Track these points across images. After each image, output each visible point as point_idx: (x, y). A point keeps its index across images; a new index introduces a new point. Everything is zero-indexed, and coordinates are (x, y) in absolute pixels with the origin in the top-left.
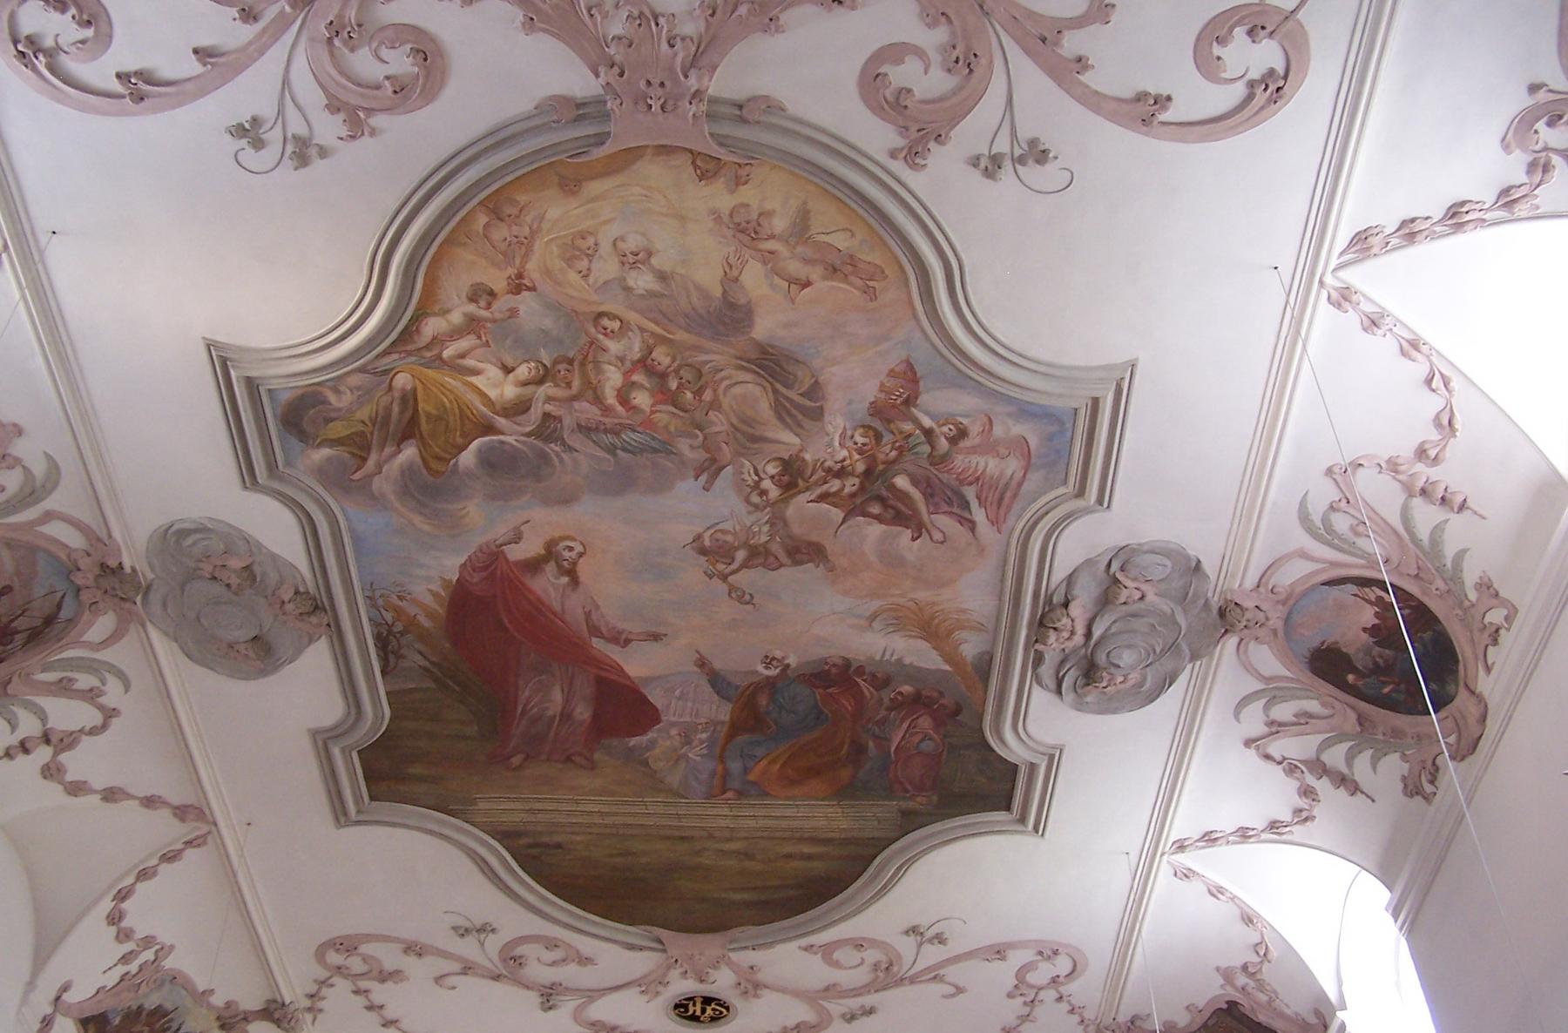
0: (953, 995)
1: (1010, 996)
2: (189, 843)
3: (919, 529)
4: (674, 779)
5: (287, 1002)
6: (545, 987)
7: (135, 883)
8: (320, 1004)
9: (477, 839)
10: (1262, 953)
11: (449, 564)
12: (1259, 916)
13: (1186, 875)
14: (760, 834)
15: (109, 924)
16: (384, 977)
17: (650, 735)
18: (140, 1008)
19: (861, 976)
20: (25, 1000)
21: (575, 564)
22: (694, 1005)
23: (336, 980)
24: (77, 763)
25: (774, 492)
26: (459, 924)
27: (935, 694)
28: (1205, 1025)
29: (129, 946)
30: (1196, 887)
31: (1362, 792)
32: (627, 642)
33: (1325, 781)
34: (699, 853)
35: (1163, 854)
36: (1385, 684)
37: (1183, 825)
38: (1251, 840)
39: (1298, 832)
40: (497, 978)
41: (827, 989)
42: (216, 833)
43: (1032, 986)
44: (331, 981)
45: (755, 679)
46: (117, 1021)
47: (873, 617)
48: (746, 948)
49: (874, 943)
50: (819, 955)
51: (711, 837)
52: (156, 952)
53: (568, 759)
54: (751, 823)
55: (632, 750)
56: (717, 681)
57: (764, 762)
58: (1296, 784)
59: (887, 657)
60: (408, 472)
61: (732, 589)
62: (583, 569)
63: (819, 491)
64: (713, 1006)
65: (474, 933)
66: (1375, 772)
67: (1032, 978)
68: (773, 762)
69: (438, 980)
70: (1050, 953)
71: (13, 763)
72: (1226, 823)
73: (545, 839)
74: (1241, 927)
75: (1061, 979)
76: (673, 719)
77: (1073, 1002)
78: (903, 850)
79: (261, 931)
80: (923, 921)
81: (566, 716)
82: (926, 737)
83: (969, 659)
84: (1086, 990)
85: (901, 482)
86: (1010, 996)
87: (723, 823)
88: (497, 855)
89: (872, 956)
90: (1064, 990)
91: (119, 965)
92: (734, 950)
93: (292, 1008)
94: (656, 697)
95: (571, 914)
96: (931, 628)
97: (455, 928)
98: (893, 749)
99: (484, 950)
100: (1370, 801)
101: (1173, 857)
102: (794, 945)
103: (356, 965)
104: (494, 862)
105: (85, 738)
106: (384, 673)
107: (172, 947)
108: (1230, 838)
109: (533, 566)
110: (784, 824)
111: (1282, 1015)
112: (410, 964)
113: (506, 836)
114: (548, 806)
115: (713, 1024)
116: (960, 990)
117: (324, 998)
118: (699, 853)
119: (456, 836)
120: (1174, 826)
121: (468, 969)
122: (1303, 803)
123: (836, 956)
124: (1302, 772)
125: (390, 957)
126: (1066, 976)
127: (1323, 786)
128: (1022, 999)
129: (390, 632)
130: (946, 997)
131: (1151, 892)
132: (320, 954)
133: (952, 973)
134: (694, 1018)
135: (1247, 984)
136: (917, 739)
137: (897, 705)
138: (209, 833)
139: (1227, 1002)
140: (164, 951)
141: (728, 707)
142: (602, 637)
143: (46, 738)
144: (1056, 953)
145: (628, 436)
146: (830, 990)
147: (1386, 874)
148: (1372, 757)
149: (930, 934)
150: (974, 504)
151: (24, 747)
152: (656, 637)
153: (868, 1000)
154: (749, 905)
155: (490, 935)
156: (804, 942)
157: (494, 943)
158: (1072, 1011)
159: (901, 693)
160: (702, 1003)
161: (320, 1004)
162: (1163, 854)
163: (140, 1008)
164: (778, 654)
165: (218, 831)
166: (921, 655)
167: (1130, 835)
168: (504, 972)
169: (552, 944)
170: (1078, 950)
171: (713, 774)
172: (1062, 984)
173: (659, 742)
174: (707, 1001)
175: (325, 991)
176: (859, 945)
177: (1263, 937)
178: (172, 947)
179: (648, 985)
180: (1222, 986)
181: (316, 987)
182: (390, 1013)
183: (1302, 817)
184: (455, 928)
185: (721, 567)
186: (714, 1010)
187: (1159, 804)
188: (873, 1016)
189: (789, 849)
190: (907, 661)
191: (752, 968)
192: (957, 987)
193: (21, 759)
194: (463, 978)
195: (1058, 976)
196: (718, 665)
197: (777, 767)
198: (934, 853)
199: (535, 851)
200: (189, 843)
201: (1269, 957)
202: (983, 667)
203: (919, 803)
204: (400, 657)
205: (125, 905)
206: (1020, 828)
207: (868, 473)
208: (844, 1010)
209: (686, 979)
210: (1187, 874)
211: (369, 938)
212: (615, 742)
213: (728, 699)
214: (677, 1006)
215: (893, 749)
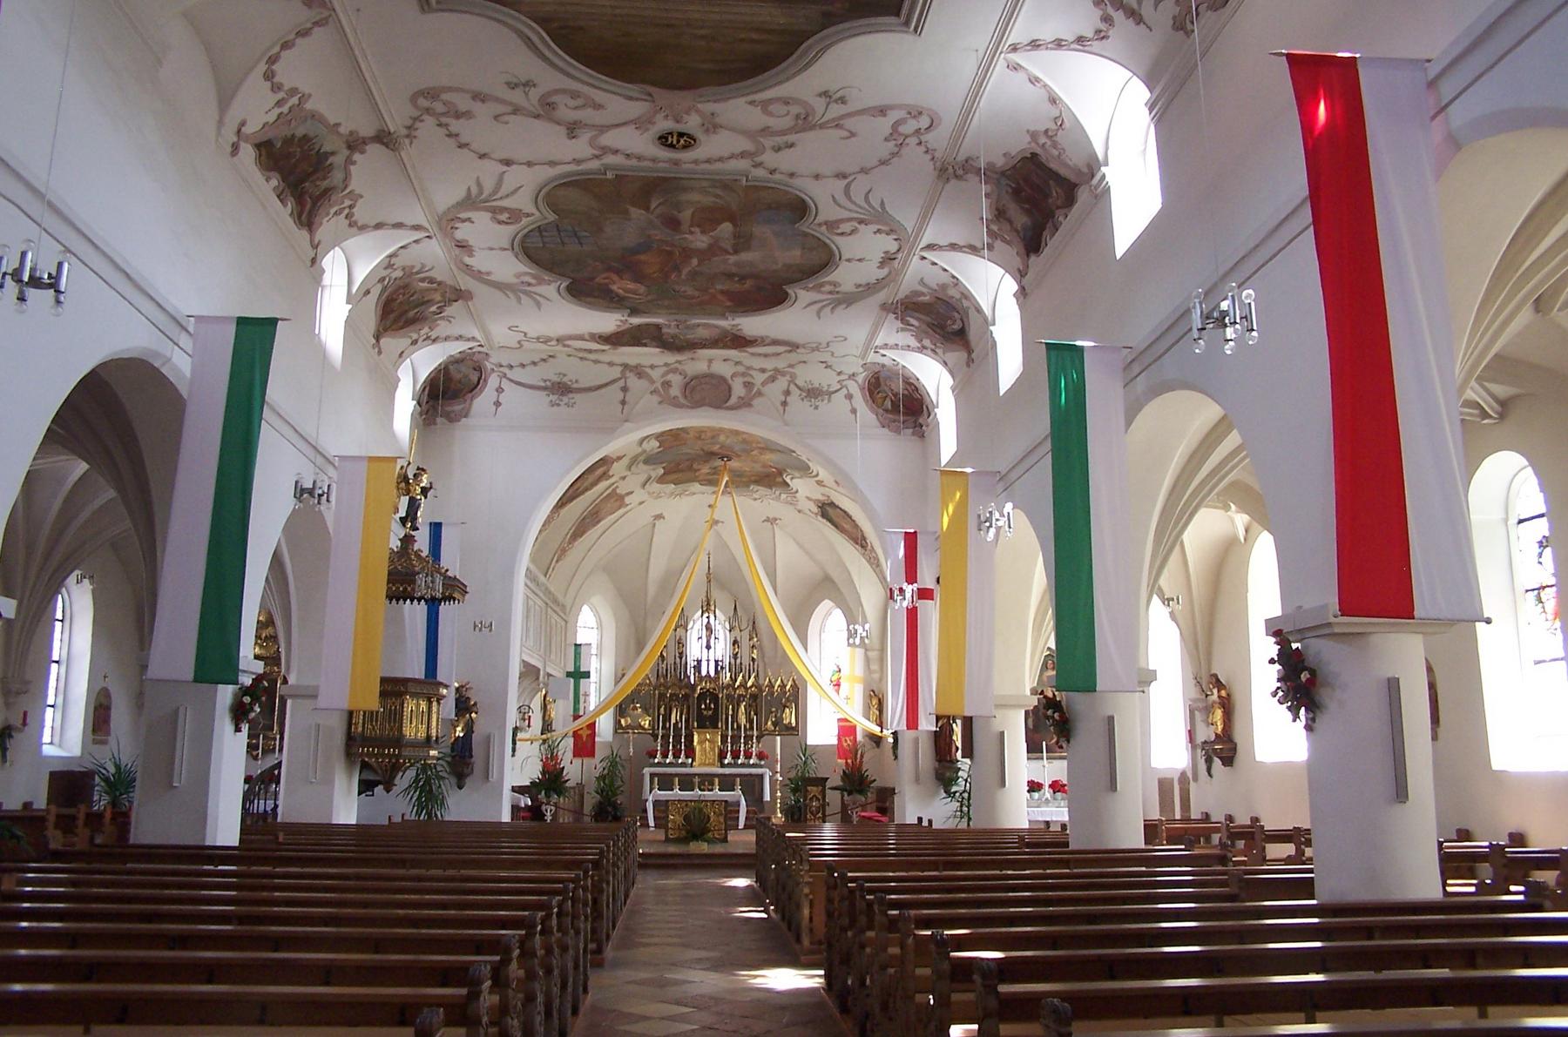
0: (847, 138)
1: (886, 139)
2: (316, 24)
5: (392, 131)
6: (570, 124)
7: (281, 51)
8: (414, 133)
9: (524, 23)
10: (1059, 124)
12: (1060, 99)
13: (1015, 68)
15: (265, 80)
16: (458, 115)
19: (787, 122)
20: (219, 133)
22: (672, 137)
23: (425, 117)
26: (510, 80)
28: (1014, 167)
29: (281, 95)
30: (1021, 76)
31: (1144, 23)
33: (1121, 12)
35: (1001, 53)
37: (1017, 34)
38: (1064, 48)
39: (1096, 46)
40: (537, 117)
41: (763, 130)
42: (334, 16)
43: (900, 134)
44: (421, 118)
46: (279, 145)
48: (709, 101)
49: (797, 101)
50: (759, 108)
52: (300, 98)
58: (1101, 13)
64: (685, 138)
65: (522, 87)
66: (1156, 10)
67: (901, 129)
69: (496, 117)
70: (916, 113)
72: (1047, 35)
74: (1047, 105)
75: (922, 131)
77: (929, 146)
78: (822, 39)
80: (833, 87)
84: (939, 139)
86: (886, 139)
88: (538, 34)
89: (795, 109)
90: (923, 138)
91: (276, 108)
92: (700, 102)
93: (395, 136)
95: (587, 74)
97: (508, 84)
100: (1148, 30)
101: (1009, 55)
102: (741, 101)
103: (439, 107)
104: (535, 39)
107: (310, 95)
108: (1049, 46)
111: (1066, 165)
112: (477, 108)
113: (543, 21)
115: (685, 150)
116: (853, 135)
117: (417, 129)
119: (510, 21)
121: (516, 111)
122: (1103, 26)
123: (771, 108)
124: (1106, 5)
125: (463, 103)
126: (926, 129)
127: (1118, 16)
128: (894, 142)
130: (844, 138)
131: (996, 64)
132: (414, 99)
133: (848, 123)
134: (672, 146)
135: (1046, 143)
138: (330, 16)
139: (1031, 153)
140: (304, 98)
144: (920, 113)
146: (766, 131)
147: (1149, 82)
149: (834, 97)
153: (791, 138)
155: (533, 88)
156: (750, 98)
157: (535, 94)
158: (927, 152)
160: (678, 136)
161: (414, 133)
163: (293, 135)
165: (336, 15)
167: (981, 39)
168: (542, 113)
169: (575, 95)
170: (936, 113)
172: (922, 134)
174: (681, 135)
175: (418, 124)
176: (786, 102)
177: (1061, 113)
178: (310, 95)
179: (640, 123)
180: (1029, 143)
181: (411, 122)
182: (463, 140)
183: (1101, 35)
184: (508, 84)
186: (685, 141)
187: (1000, 26)
188: (792, 149)
191: (713, 114)
192: (851, 132)
194: (513, 117)
195: (920, 129)
198: (843, 43)
200: (316, 24)
201: (1063, 127)
206: (905, 29)
208: (772, 144)
209: (667, 119)
210: (1016, 67)
211: (450, 89)
214: (660, 138)
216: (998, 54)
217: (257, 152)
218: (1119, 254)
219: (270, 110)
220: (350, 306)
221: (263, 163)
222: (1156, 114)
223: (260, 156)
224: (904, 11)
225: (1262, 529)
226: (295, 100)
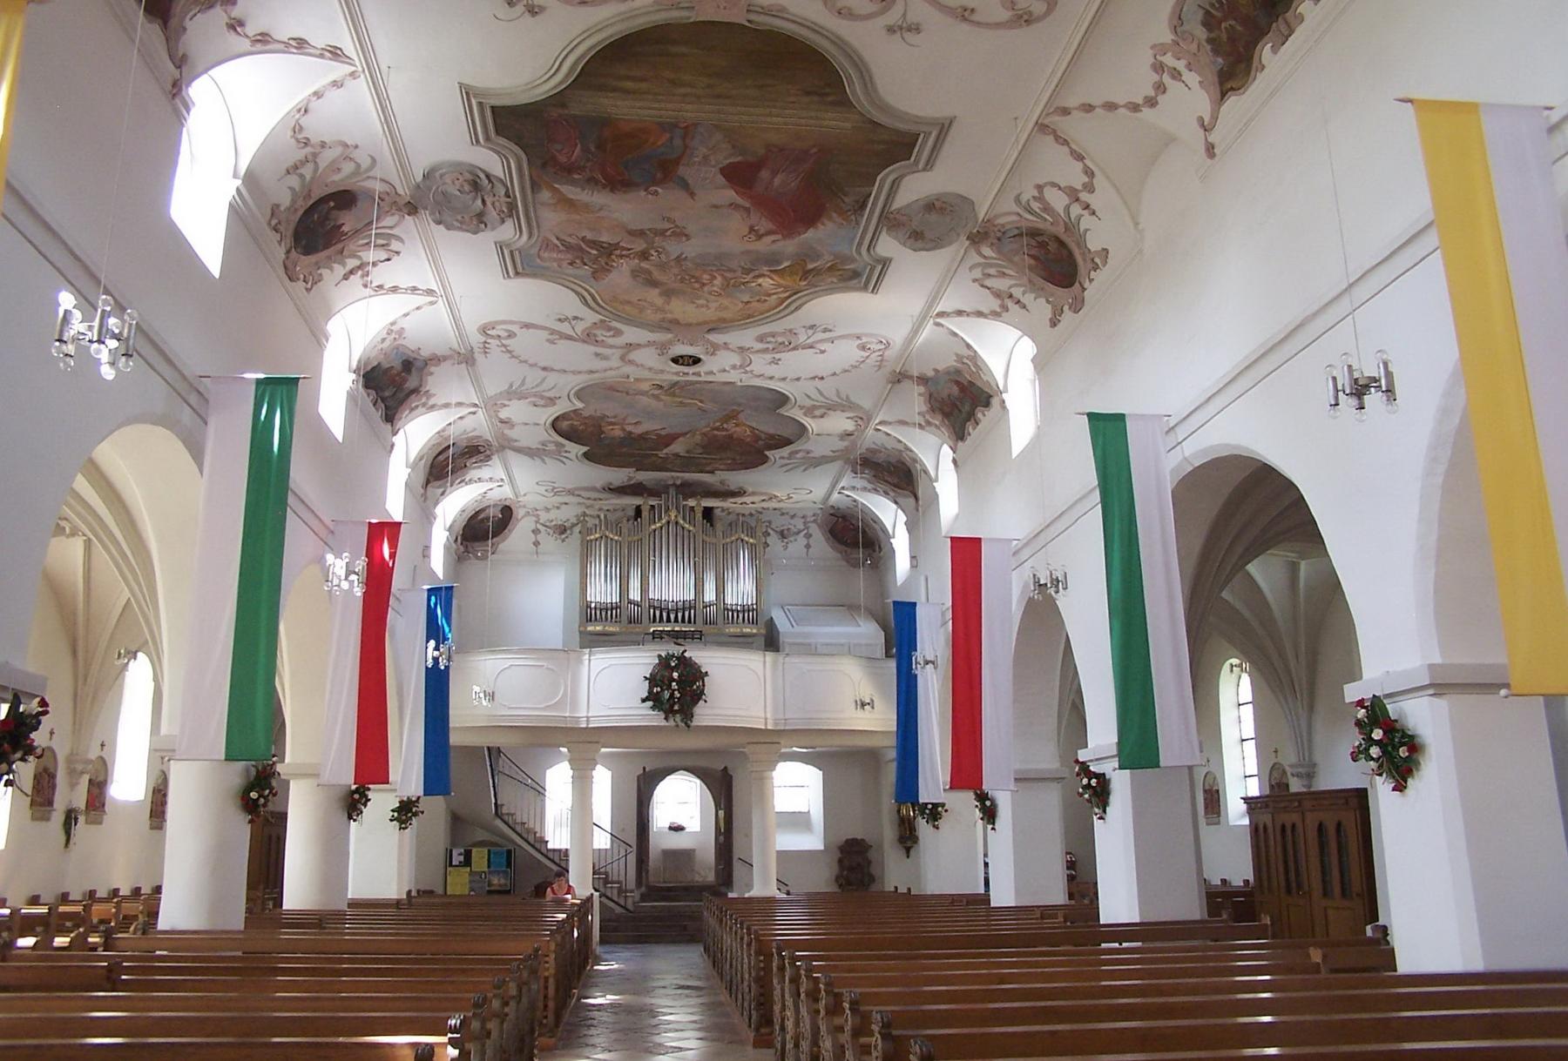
7: (1121, 106)
17: (728, 161)
18: (1209, 41)
21: (750, 233)
24: (1078, 180)
27: (559, 172)
34: (709, 86)
36: (318, 218)
47: (601, 209)
53: (781, 150)
54: (669, 106)
55: (740, 155)
56: (685, 186)
57: (659, 143)
59: (590, 192)
60: (813, 261)
63: (631, 251)
71: (1097, 210)
73: (816, 98)
76: (713, 169)
81: (774, 173)
82: (560, 151)
85: (595, 252)
87: (689, 107)
88: (855, 90)
91: (1183, 78)
94: (721, 180)
96: (570, 204)
99: (905, 10)
100: (279, 177)
105: (1062, 186)
113: (844, 103)
118: (709, 86)
120: (373, 105)
129: (855, 211)
140: (1159, 49)
141: (679, 173)
142: (743, 207)
145: (714, 269)
148: (295, 190)
150: (559, 245)
151: (1087, 207)
152: (716, 207)
159: (579, 174)
162: (364, 71)
166: (569, 191)
171: (693, 138)
173: (725, 157)
183: (297, 129)
185: (678, 230)
189: (644, 86)
197: (652, 140)
202: (535, 186)
203: (555, 113)
204: (857, 202)
207: (611, 254)
216: (365, 66)
217: (1229, 93)
218: (340, 439)
219: (1187, 85)
221: (1240, 84)
222: (238, 205)
223: (1232, 89)
224: (488, 113)
225: (452, 754)
226: (1169, 60)
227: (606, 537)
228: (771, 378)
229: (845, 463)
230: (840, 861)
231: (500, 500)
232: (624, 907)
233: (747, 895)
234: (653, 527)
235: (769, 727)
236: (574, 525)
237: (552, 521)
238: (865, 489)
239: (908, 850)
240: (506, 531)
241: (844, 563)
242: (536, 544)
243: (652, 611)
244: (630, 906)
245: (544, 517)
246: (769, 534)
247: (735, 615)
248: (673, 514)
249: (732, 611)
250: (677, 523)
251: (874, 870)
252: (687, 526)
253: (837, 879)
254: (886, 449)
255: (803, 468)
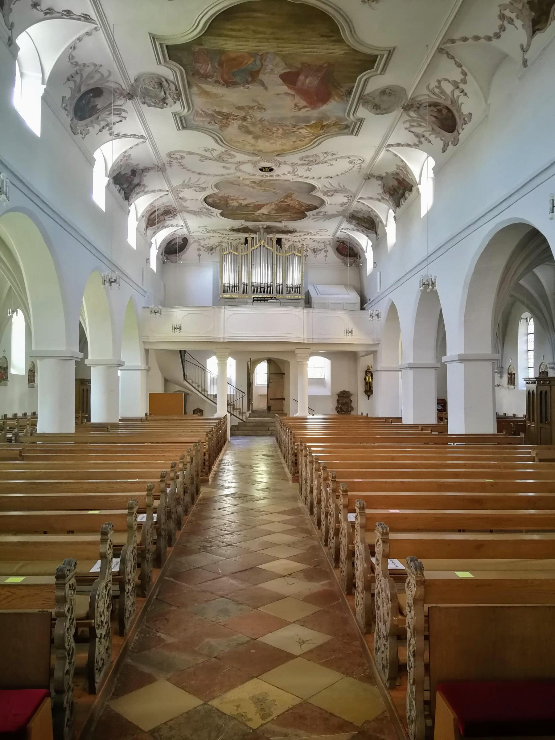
3: (214, 111)
4: (278, 59)
11: (325, 107)
14: (250, 40)
25: (248, 117)
32: (285, 93)
34: (272, 33)
45: (252, 84)
51: (268, 39)
53: (309, 65)
55: (289, 68)
56: (262, 84)
61: (258, 102)
62: (293, 106)
68: (247, 63)
73: (326, 39)
79: (453, 17)
81: (306, 77)
83: (194, 86)
94: (281, 81)
96: (206, 93)
98: (210, 65)
105: (450, 80)
106: (354, 87)
109: (305, 107)
110: (242, 43)
113: (340, 41)
114: (320, 50)
136: (203, 67)
137: (211, 76)
143: (458, 87)
150: (203, 114)
154: (255, 11)
164: (246, 90)
171: (265, 60)
173: (282, 69)
183: (71, 57)
190: (211, 86)
193: (465, 91)
196: (262, 88)
197: (245, 62)
199: (331, 34)
203: (197, 48)
205: (492, 35)
212: (294, 70)
213: (260, 80)
215: (210, 65)
220: (138, 222)
227: (232, 253)
228: (307, 178)
229: (344, 217)
230: (338, 400)
231: (182, 235)
232: (242, 420)
233: (295, 415)
234: (253, 248)
235: (305, 342)
236: (217, 247)
237: (206, 245)
238: (353, 229)
239: (369, 396)
240: (185, 249)
241: (343, 264)
242: (199, 255)
243: (253, 288)
244: (244, 419)
245: (203, 243)
246: (308, 251)
247: (291, 289)
248: (262, 242)
249: (290, 288)
250: (264, 246)
251: (353, 404)
252: (269, 247)
253: (336, 408)
254: (363, 210)
255: (324, 220)
